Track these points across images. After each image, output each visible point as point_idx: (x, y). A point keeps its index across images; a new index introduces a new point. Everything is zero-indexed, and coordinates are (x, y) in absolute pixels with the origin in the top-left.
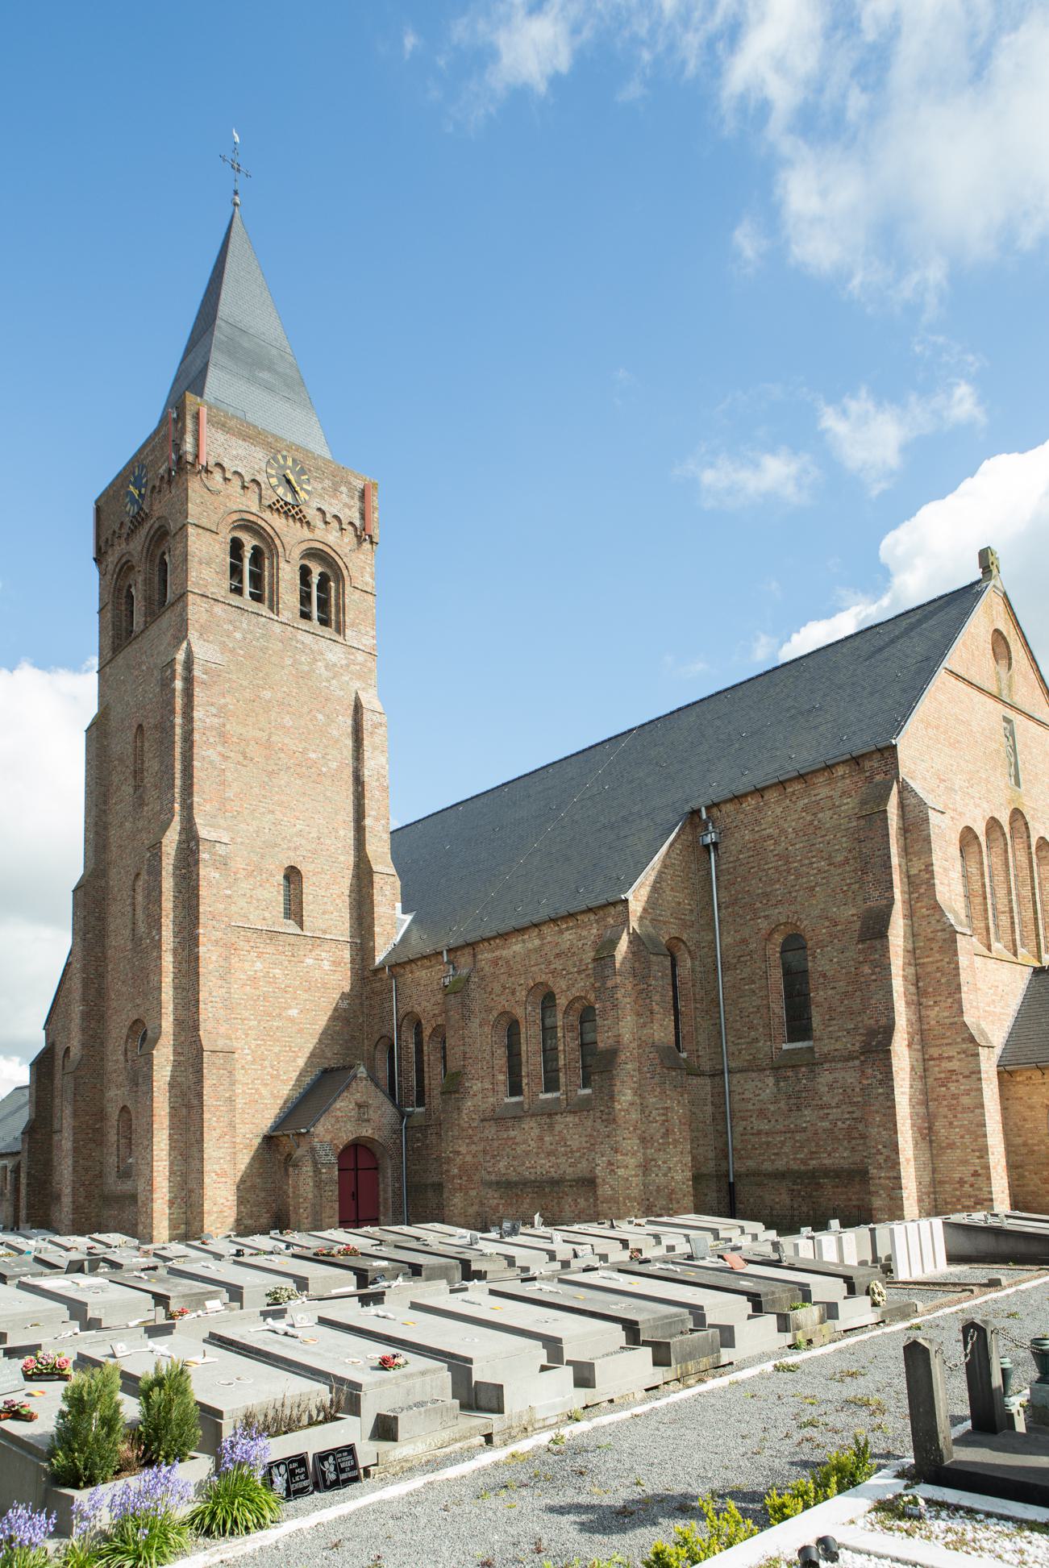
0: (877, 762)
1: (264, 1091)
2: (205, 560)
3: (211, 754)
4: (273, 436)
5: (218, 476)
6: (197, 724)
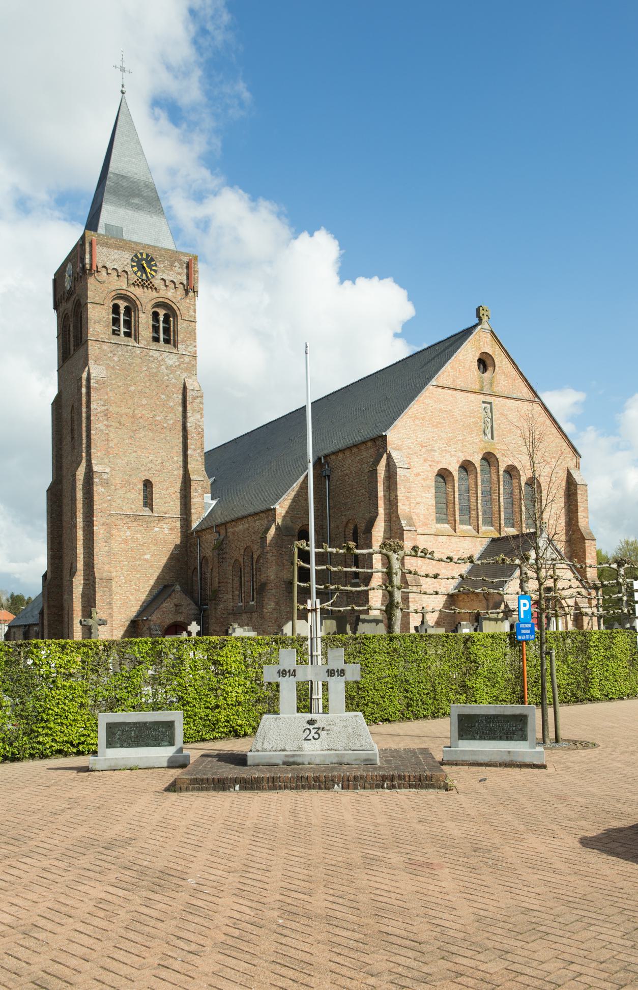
0: (380, 443)
1: (131, 598)
2: (98, 318)
3: (101, 426)
4: (135, 243)
5: (104, 272)
6: (93, 411)
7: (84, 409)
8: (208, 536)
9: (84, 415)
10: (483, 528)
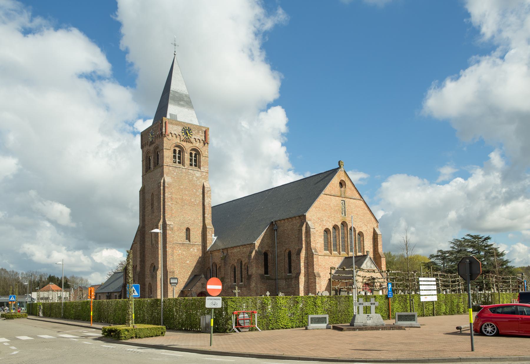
0: (303, 218)
2: (168, 155)
3: (169, 204)
5: (170, 135)
6: (166, 197)
7: (162, 196)
8: (217, 254)
9: (162, 199)
10: (342, 253)
